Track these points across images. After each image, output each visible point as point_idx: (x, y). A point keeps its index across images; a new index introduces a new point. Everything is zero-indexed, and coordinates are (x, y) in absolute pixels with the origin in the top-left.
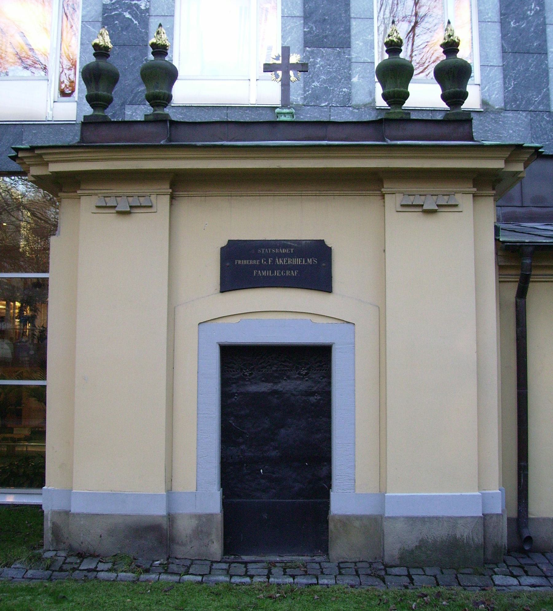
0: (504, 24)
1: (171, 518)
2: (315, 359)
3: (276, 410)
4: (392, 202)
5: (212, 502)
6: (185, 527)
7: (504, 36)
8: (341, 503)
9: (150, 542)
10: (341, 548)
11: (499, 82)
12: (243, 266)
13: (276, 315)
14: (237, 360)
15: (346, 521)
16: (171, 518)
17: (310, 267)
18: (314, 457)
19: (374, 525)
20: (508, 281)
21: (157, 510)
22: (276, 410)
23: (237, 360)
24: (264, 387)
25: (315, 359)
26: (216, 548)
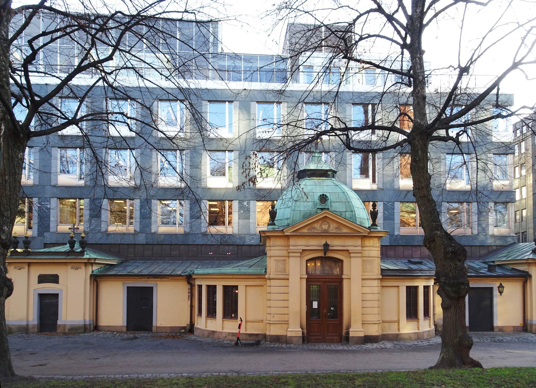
0: (141, 211)
1: (27, 325)
2: (56, 296)
3: (48, 305)
4: (69, 267)
5: (36, 322)
6: (30, 327)
7: (140, 214)
8: (59, 322)
9: (25, 330)
10: (59, 330)
11: (139, 226)
12: (42, 279)
13: (49, 288)
14: (42, 297)
15: (60, 325)
16: (27, 325)
17: (55, 279)
18: (55, 314)
19: (64, 326)
20: (278, 257)
21: (24, 323)
22: (48, 305)
23: (42, 297)
24: (48, 301)
25: (56, 296)
26: (36, 330)
